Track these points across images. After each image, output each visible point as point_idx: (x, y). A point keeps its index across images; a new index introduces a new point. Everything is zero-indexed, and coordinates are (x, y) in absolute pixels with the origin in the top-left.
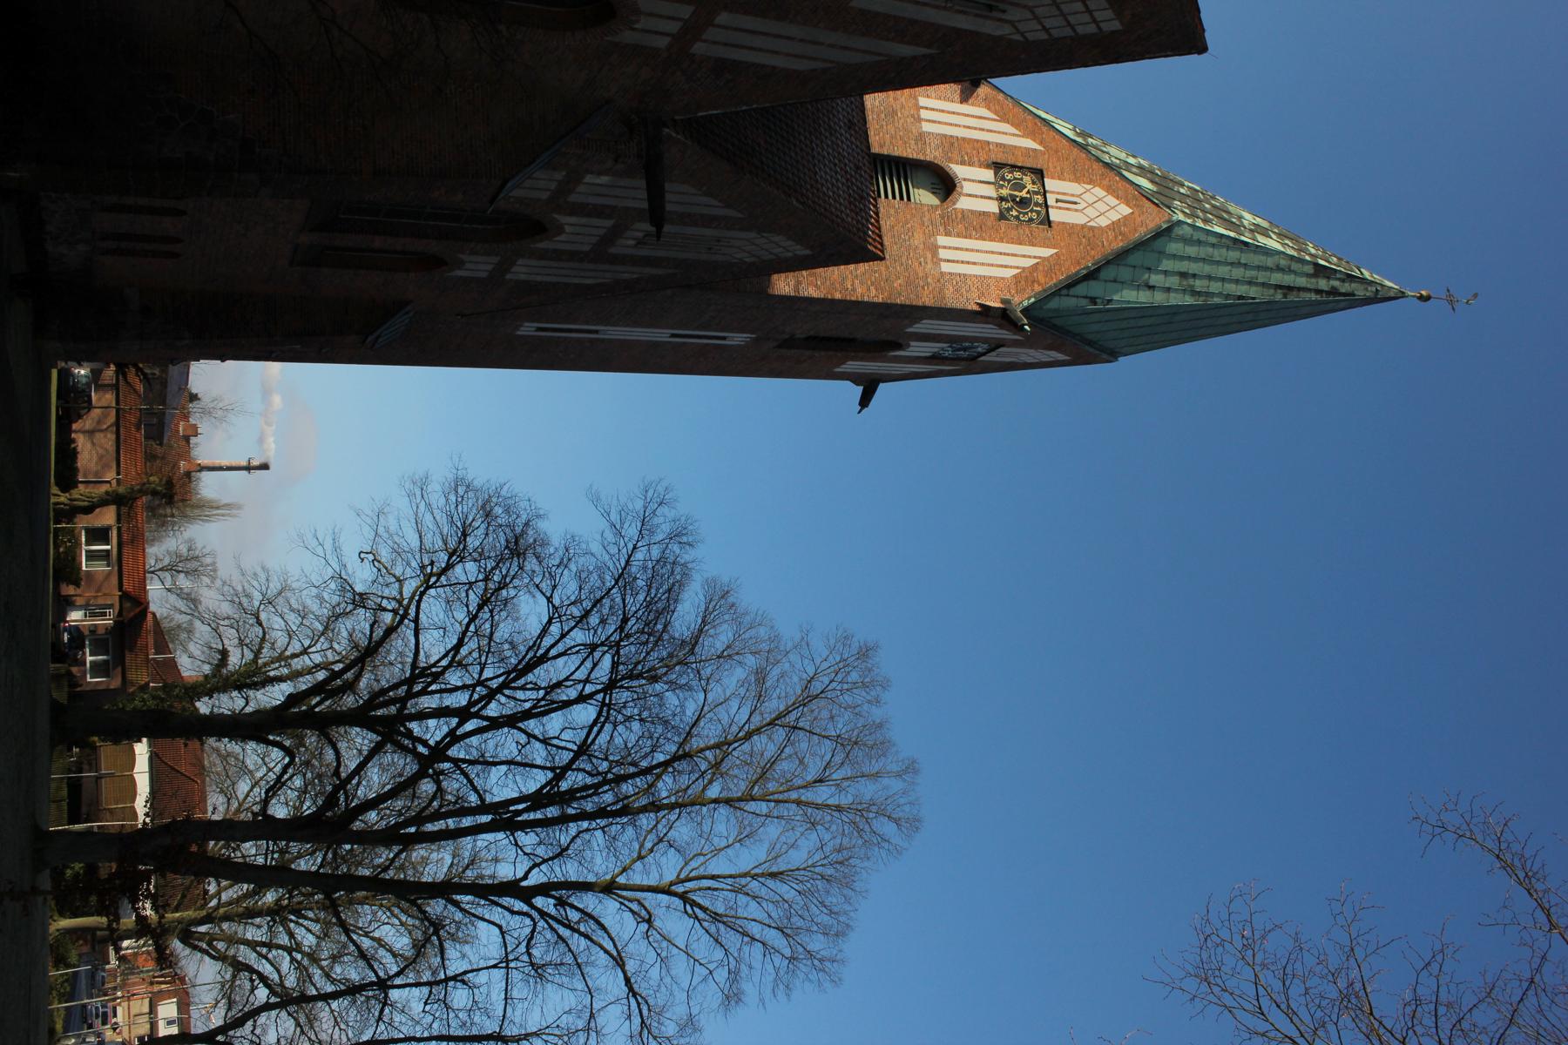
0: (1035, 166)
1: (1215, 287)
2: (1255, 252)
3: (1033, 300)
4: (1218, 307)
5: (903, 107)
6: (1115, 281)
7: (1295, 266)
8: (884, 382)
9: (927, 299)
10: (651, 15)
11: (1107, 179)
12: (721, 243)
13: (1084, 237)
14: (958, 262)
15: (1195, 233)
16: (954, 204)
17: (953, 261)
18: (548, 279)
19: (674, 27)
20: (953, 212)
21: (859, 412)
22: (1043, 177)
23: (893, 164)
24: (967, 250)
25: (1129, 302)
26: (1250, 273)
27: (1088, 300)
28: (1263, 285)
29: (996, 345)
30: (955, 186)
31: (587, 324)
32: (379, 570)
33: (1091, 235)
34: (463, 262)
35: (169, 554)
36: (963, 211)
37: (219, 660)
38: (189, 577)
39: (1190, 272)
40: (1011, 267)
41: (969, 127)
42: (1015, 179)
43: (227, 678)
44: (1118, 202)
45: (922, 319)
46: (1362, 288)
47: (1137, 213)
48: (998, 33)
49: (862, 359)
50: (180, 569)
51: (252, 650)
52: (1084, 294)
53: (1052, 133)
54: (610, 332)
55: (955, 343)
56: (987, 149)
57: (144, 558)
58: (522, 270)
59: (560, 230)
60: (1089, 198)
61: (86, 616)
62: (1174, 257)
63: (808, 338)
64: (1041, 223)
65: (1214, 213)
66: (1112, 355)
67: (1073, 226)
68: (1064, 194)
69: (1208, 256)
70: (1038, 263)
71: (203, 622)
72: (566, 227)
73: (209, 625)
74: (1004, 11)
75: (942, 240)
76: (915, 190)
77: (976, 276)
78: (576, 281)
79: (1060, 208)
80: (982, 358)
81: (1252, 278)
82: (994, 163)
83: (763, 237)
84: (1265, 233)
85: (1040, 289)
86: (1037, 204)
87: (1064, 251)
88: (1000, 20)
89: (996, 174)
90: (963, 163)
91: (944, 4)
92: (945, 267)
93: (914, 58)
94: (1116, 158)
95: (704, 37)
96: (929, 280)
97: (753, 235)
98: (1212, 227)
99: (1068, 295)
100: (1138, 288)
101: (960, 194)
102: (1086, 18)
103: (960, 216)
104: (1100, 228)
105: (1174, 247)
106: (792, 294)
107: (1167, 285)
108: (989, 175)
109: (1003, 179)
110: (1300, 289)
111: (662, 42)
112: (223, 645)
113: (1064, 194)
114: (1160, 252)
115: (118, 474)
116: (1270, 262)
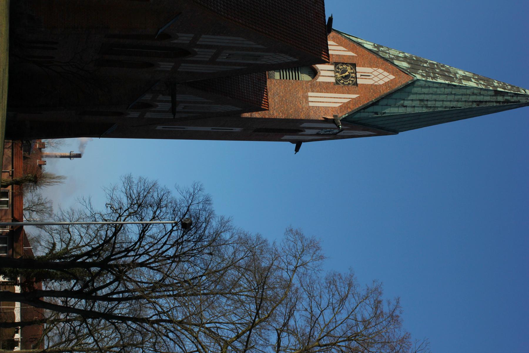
0: (352, 63)
1: (438, 104)
2: (460, 88)
3: (347, 115)
4: (441, 112)
7: (482, 92)
8: (304, 142)
9: (302, 117)
11: (385, 65)
14: (316, 102)
15: (426, 84)
16: (316, 80)
20: (316, 83)
21: (295, 154)
24: (320, 97)
25: (394, 113)
26: (457, 97)
28: (465, 101)
30: (317, 73)
33: (375, 88)
35: (29, 202)
36: (320, 82)
37: (52, 247)
38: (38, 214)
39: (425, 99)
40: (339, 103)
42: (343, 68)
43: (55, 254)
50: (34, 209)
51: (66, 244)
53: (361, 48)
58: (148, 115)
59: (157, 106)
62: (416, 93)
64: (353, 85)
69: (433, 92)
70: (350, 101)
71: (46, 231)
73: (49, 232)
75: (310, 94)
76: (302, 75)
79: (362, 78)
80: (338, 134)
81: (459, 99)
82: (334, 63)
84: (468, 79)
85: (351, 110)
86: (352, 77)
87: (362, 95)
89: (335, 67)
92: (311, 104)
94: (393, 55)
98: (437, 80)
99: (364, 112)
100: (398, 107)
101: (319, 76)
103: (318, 84)
105: (415, 90)
106: (249, 117)
107: (413, 105)
108: (332, 67)
109: (338, 68)
110: (486, 102)
112: (54, 241)
114: (409, 93)
115: (13, 168)
116: (468, 92)
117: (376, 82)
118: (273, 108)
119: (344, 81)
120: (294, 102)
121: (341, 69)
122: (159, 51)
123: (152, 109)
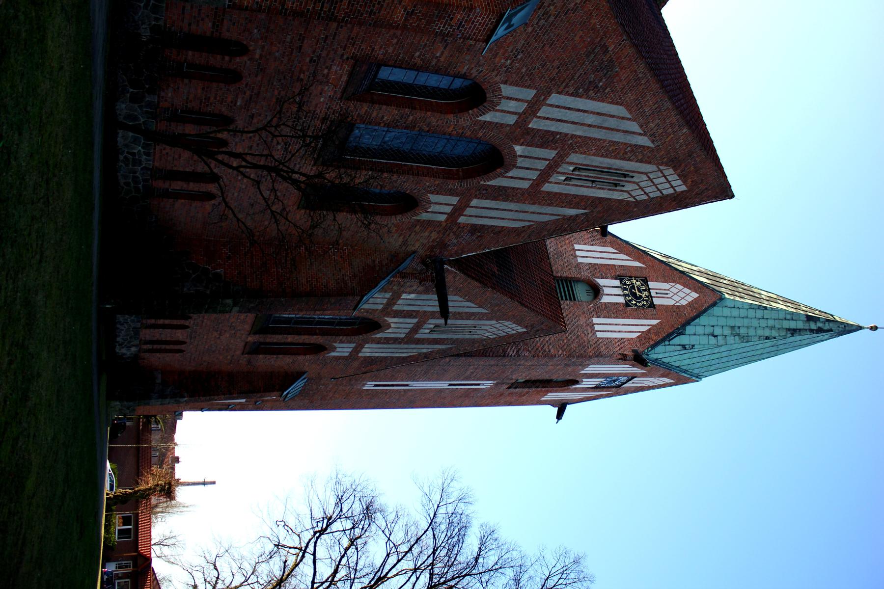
5: (566, 251)
6: (695, 335)
8: (569, 404)
10: (436, 203)
12: (476, 328)
13: (674, 312)
16: (600, 300)
17: (603, 331)
18: (382, 355)
19: (448, 209)
21: (557, 423)
22: (647, 281)
23: (564, 281)
27: (681, 347)
29: (632, 377)
31: (402, 381)
32: (288, 531)
34: (335, 348)
36: (605, 303)
40: (636, 332)
41: (603, 258)
44: (691, 291)
45: (589, 365)
46: (836, 326)
47: (702, 297)
48: (621, 198)
49: (556, 392)
52: (679, 344)
54: (414, 385)
55: (608, 378)
56: (615, 269)
57: (255, 321)
58: (368, 351)
59: (389, 326)
60: (674, 290)
61: (116, 569)
63: (527, 382)
65: (745, 293)
66: (698, 377)
67: (667, 306)
68: (660, 289)
72: (391, 324)
74: (623, 186)
75: (595, 320)
77: (617, 338)
78: (397, 355)
79: (659, 297)
80: (623, 386)
83: (499, 323)
88: (622, 191)
89: (621, 282)
90: (602, 278)
91: (591, 185)
92: (599, 335)
93: (577, 216)
95: (464, 213)
96: (591, 343)
97: (494, 322)
99: (669, 345)
102: (667, 185)
103: (604, 307)
104: (683, 306)
108: (617, 283)
109: (625, 284)
111: (443, 218)
113: (660, 289)
117: (677, 302)
118: (547, 342)
119: (637, 302)
120: (576, 332)
121: (629, 285)
122: (433, 167)
123: (378, 336)
